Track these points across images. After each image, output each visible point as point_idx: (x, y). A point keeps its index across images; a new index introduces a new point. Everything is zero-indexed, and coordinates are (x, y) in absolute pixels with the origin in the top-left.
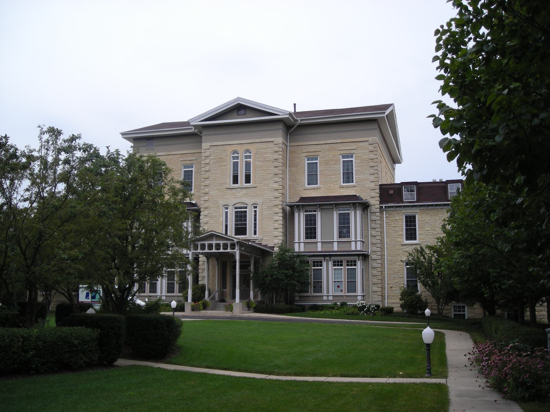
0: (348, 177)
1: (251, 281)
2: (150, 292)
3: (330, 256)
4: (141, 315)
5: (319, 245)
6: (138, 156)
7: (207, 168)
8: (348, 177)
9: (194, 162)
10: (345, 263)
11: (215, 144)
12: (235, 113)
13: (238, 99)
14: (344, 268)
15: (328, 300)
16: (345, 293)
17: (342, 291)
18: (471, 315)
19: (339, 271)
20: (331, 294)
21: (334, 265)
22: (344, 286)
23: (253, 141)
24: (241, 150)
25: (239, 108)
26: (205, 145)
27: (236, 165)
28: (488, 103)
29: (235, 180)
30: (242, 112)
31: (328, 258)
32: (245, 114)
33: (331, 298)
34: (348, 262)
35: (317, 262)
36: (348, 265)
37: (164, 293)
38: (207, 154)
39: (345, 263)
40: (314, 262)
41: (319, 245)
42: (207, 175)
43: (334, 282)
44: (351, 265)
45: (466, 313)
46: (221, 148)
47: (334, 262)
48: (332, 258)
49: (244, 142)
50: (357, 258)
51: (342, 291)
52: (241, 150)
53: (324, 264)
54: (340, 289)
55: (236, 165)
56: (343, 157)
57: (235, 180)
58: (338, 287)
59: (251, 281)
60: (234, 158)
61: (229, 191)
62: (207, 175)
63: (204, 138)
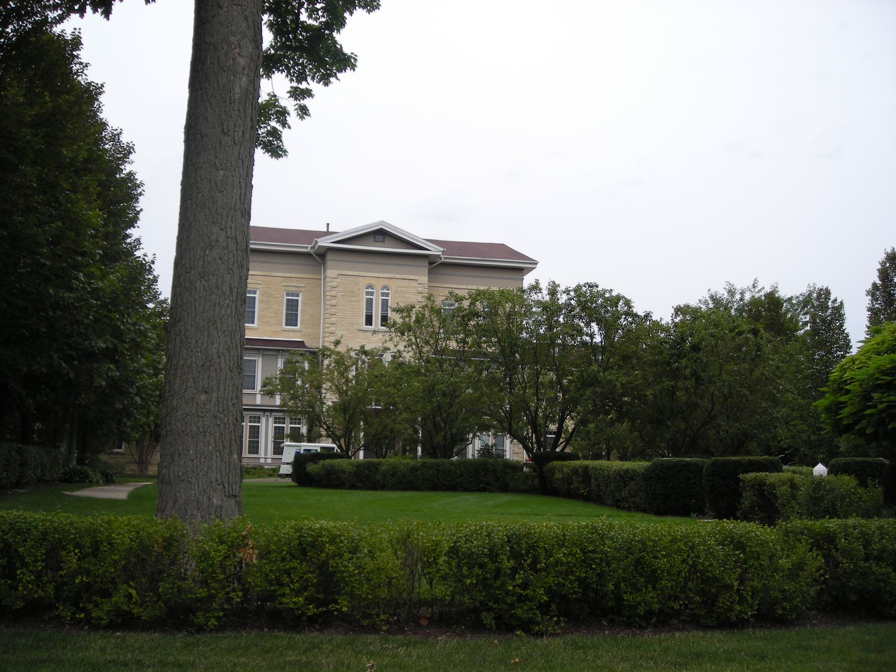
0: (292, 320)
2: (249, 453)
3: (271, 411)
5: (259, 397)
7: (334, 302)
8: (292, 320)
9: (302, 289)
11: (344, 272)
12: (371, 240)
13: (382, 222)
21: (275, 423)
23: (392, 276)
24: (378, 284)
25: (381, 234)
26: (331, 273)
27: (369, 303)
29: (369, 320)
30: (387, 239)
31: (268, 413)
32: (384, 242)
34: (251, 417)
37: (270, 454)
38: (334, 284)
41: (259, 397)
42: (333, 310)
46: (352, 278)
47: (275, 418)
49: (381, 275)
50: (261, 413)
52: (378, 284)
53: (263, 420)
55: (369, 303)
56: (288, 295)
57: (369, 321)
60: (383, 294)
61: (361, 334)
62: (333, 310)
63: (329, 264)
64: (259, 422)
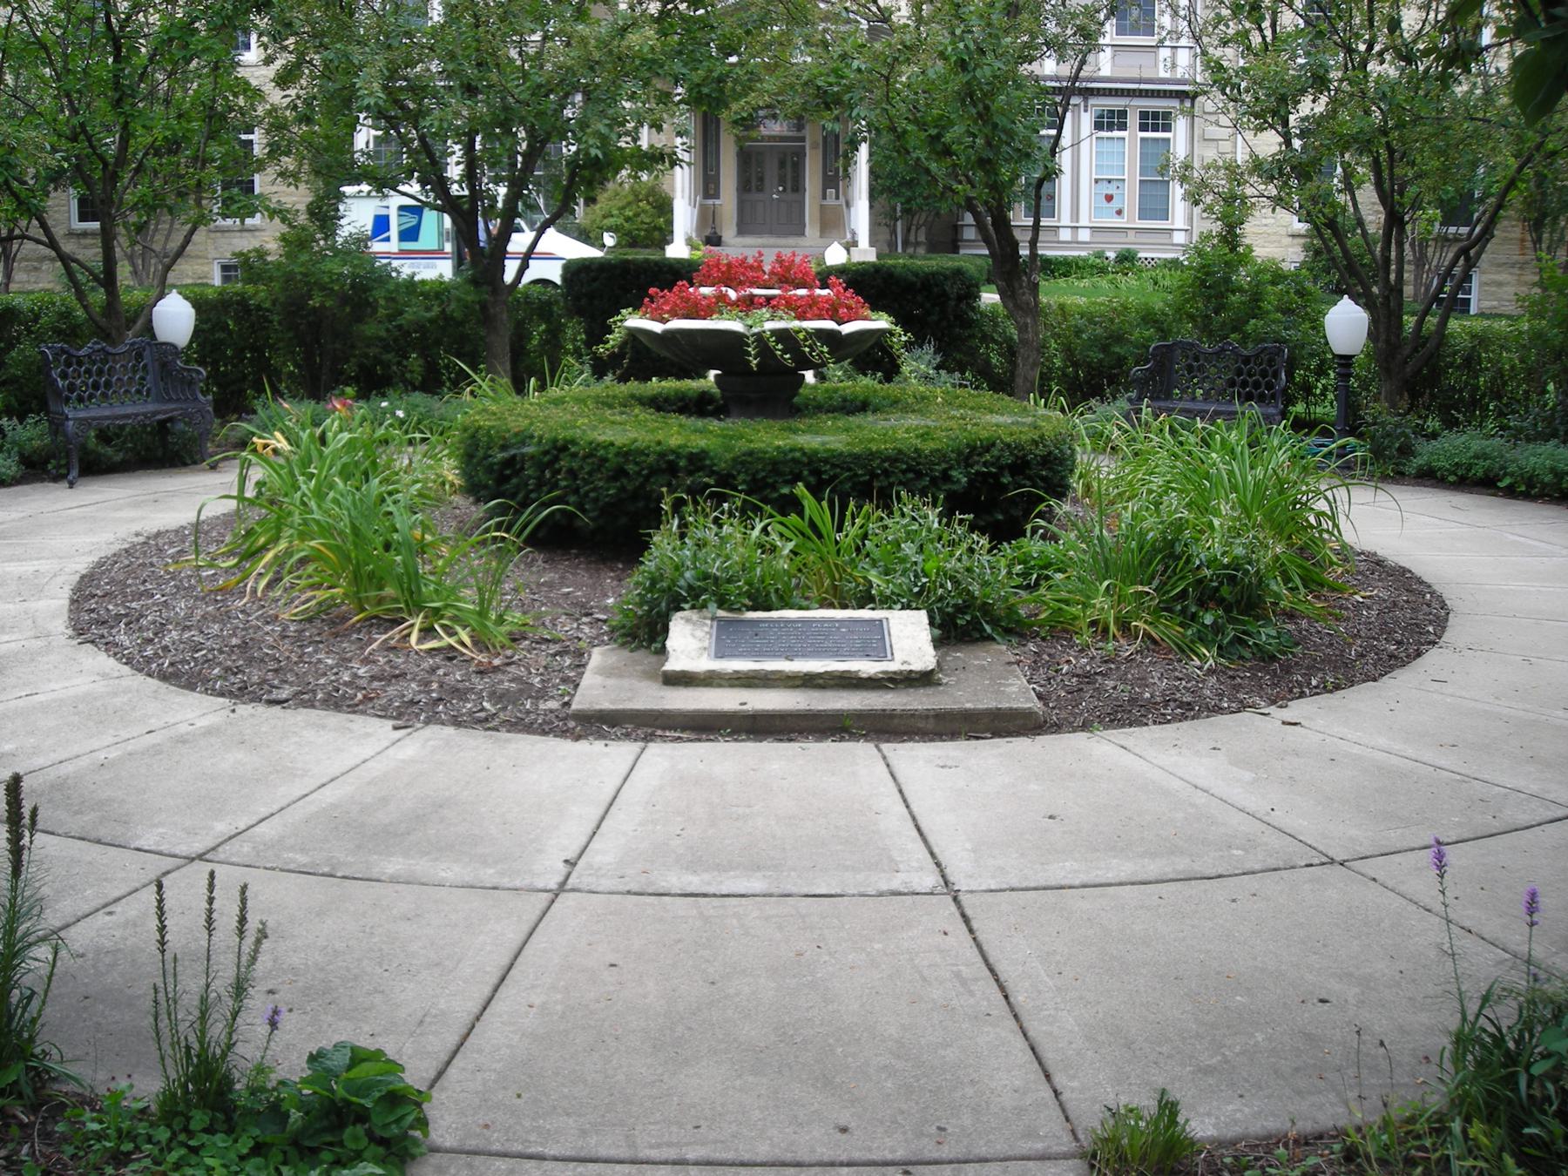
1: (864, 149)
4: (481, 225)
6: (1474, 68)
10: (1133, 120)
14: (1132, 136)
15: (1075, 243)
16: (1131, 219)
17: (1119, 212)
18: (1486, 304)
19: (1116, 146)
20: (1084, 221)
22: (1129, 197)
28: (1542, 1118)
33: (1084, 235)
34: (1144, 115)
35: (1155, 115)
36: (1143, 128)
39: (1133, 120)
40: (1144, 115)
43: (1097, 181)
44: (1155, 129)
45: (1474, 297)
48: (1092, 101)
50: (1175, 103)
51: (1119, 212)
54: (1115, 204)
58: (1109, 198)
59: (864, 149)
64: (1167, 128)
